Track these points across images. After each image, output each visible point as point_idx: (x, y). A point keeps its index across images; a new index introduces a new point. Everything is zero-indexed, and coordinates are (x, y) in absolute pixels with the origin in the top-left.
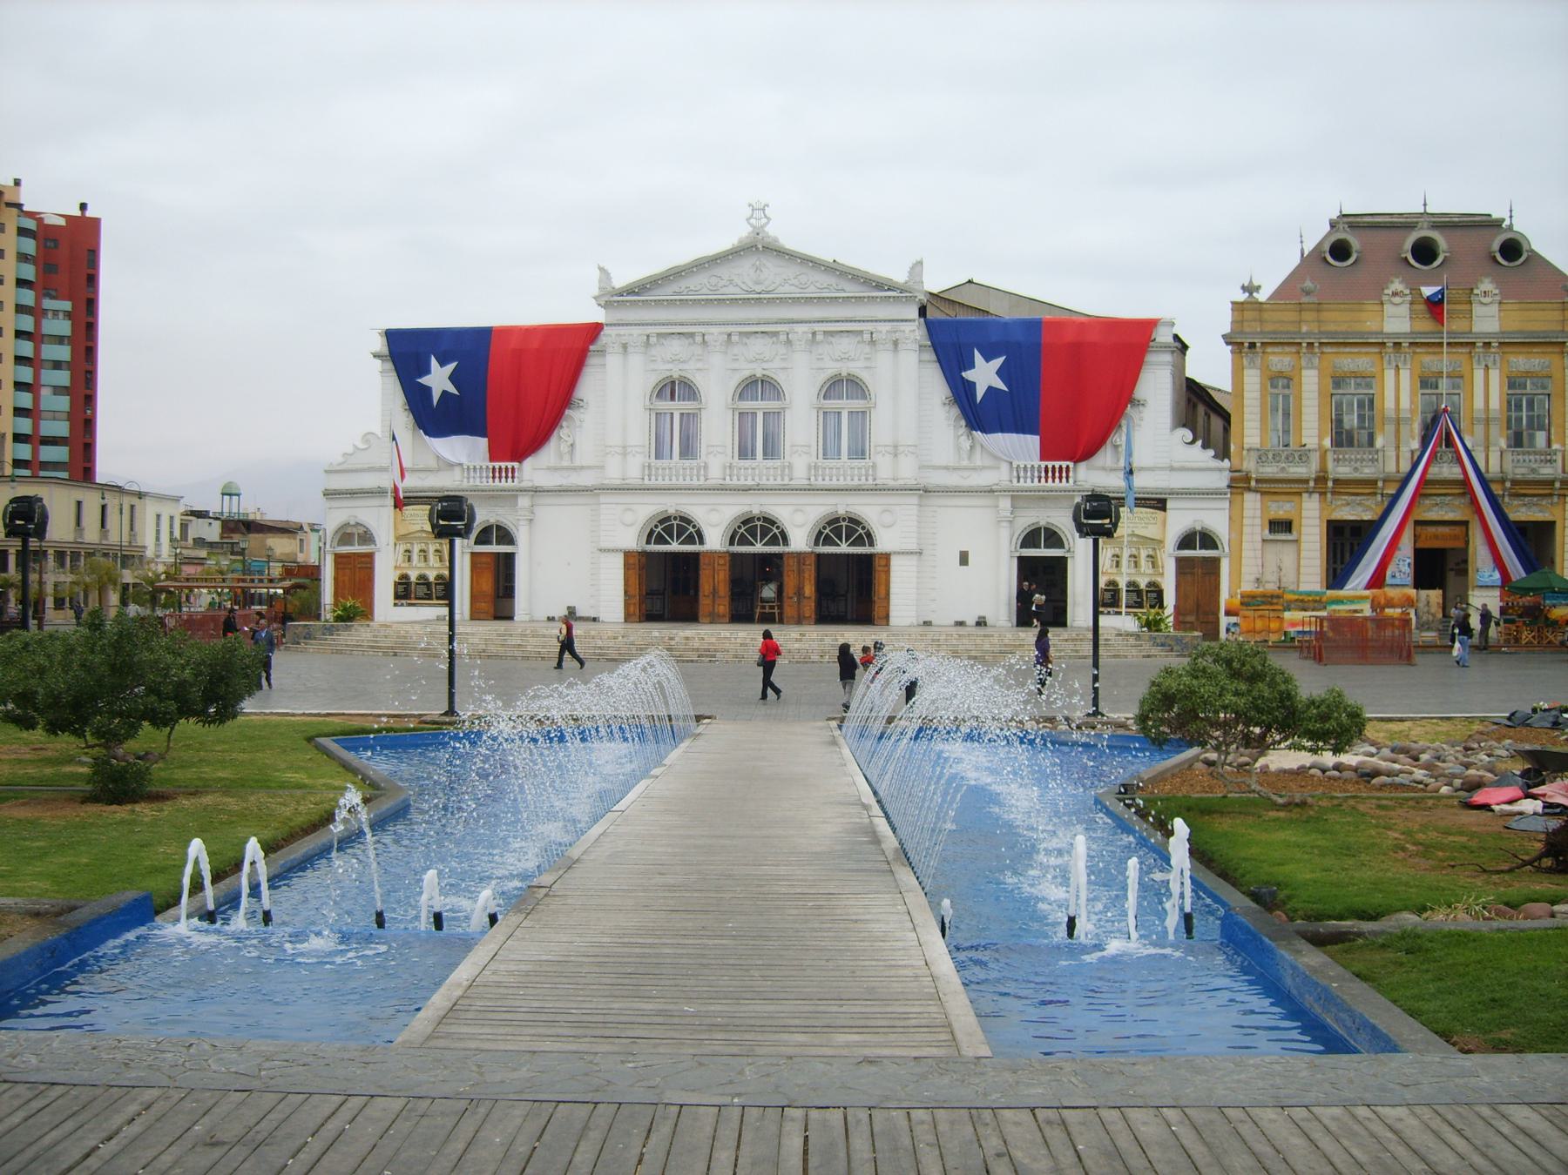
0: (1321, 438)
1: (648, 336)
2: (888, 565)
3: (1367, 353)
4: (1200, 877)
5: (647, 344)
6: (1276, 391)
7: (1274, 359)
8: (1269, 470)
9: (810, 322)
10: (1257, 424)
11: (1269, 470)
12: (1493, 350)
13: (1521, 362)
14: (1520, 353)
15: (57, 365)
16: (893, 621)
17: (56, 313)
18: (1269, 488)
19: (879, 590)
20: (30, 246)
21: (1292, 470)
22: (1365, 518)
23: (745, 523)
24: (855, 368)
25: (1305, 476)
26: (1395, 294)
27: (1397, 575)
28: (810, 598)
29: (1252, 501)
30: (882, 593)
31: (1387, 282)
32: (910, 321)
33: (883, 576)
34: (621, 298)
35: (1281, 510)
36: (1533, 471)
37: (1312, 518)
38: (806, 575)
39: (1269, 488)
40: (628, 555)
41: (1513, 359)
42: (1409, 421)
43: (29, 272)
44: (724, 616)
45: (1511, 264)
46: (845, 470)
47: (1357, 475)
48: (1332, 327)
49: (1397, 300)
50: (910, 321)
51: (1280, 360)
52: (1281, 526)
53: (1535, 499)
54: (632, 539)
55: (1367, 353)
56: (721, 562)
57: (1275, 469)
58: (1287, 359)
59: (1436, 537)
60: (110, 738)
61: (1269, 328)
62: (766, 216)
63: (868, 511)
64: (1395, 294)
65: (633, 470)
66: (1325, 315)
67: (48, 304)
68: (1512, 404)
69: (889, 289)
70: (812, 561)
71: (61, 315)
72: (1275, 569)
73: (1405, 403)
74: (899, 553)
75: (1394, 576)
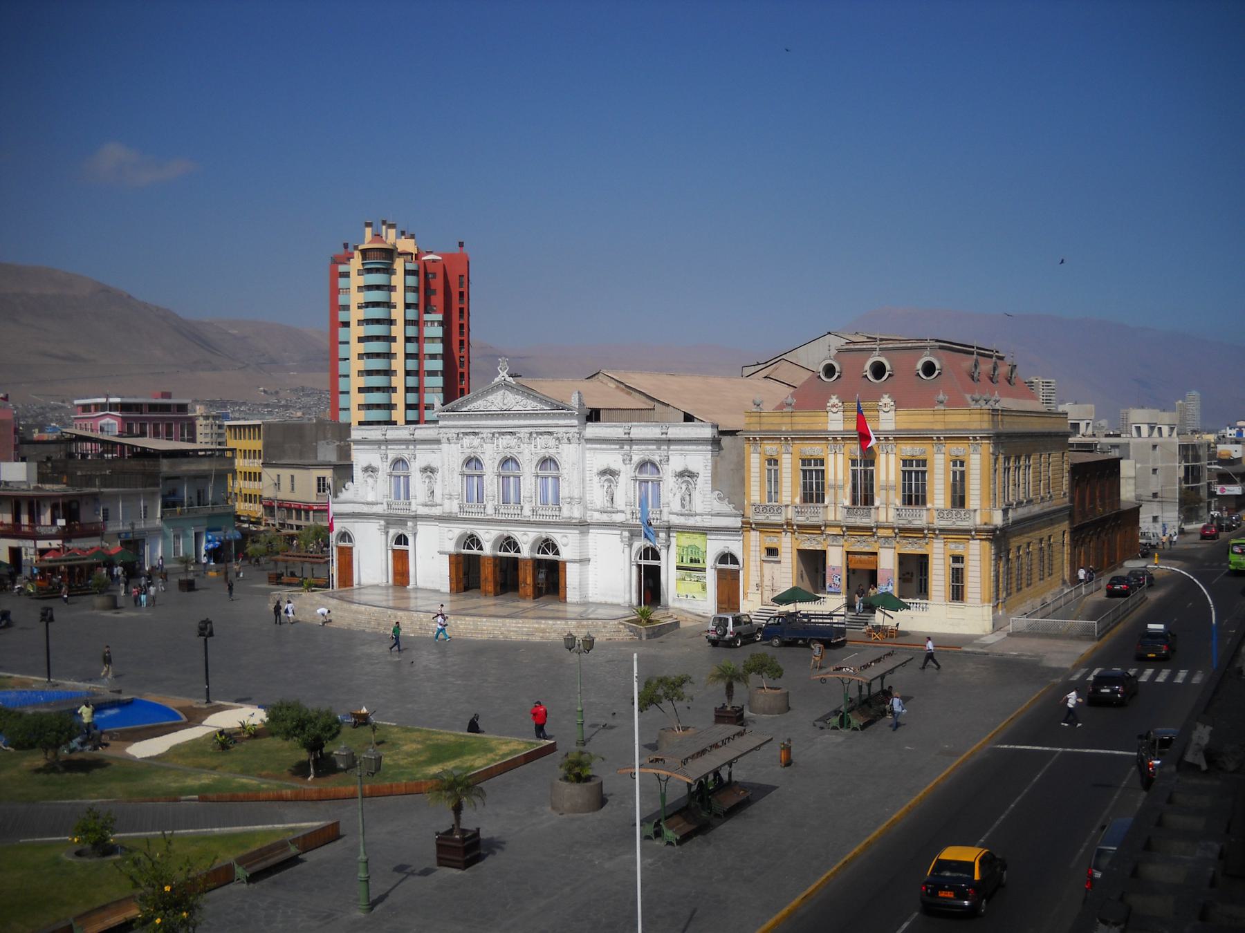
0: (793, 497)
1: (458, 434)
2: (565, 568)
3: (819, 444)
4: (1057, 755)
5: (458, 438)
6: (770, 467)
7: (768, 447)
8: (760, 517)
10: (758, 488)
11: (760, 517)
12: (890, 442)
13: (908, 449)
14: (908, 443)
15: (433, 357)
16: (568, 600)
17: (432, 322)
18: (763, 527)
19: (561, 582)
20: (412, 280)
21: (773, 518)
22: (818, 549)
24: (552, 452)
25: (779, 522)
26: (834, 406)
27: (833, 585)
28: (529, 585)
29: (754, 536)
30: (563, 585)
31: (828, 398)
32: (574, 426)
33: (563, 574)
34: (444, 413)
35: (771, 542)
36: (910, 522)
37: (787, 545)
38: (528, 572)
39: (763, 527)
40: (450, 556)
41: (903, 447)
42: (843, 487)
43: (412, 298)
44: (491, 592)
45: (929, 378)
46: (548, 514)
47: (808, 522)
48: (800, 427)
49: (835, 410)
50: (574, 426)
51: (771, 448)
52: (772, 552)
53: (915, 540)
54: (451, 547)
55: (819, 444)
56: (489, 562)
57: (763, 518)
58: (775, 447)
59: (861, 561)
60: (1217, 433)
61: (764, 428)
63: (557, 536)
64: (834, 406)
65: (452, 507)
66: (796, 419)
67: (427, 317)
68: (906, 475)
70: (530, 564)
71: (436, 324)
72: (771, 578)
73: (840, 476)
74: (572, 562)
75: (831, 587)
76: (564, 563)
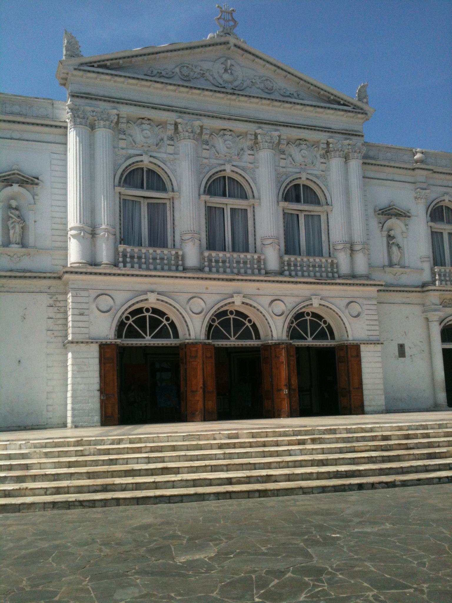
2: (358, 356)
9: (276, 125)
23: (133, 313)
40: (103, 348)
62: (233, 20)
69: (344, 105)
76: (356, 348)
